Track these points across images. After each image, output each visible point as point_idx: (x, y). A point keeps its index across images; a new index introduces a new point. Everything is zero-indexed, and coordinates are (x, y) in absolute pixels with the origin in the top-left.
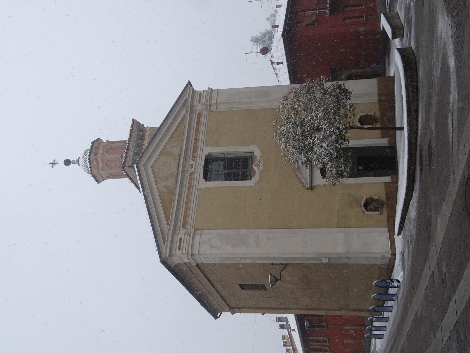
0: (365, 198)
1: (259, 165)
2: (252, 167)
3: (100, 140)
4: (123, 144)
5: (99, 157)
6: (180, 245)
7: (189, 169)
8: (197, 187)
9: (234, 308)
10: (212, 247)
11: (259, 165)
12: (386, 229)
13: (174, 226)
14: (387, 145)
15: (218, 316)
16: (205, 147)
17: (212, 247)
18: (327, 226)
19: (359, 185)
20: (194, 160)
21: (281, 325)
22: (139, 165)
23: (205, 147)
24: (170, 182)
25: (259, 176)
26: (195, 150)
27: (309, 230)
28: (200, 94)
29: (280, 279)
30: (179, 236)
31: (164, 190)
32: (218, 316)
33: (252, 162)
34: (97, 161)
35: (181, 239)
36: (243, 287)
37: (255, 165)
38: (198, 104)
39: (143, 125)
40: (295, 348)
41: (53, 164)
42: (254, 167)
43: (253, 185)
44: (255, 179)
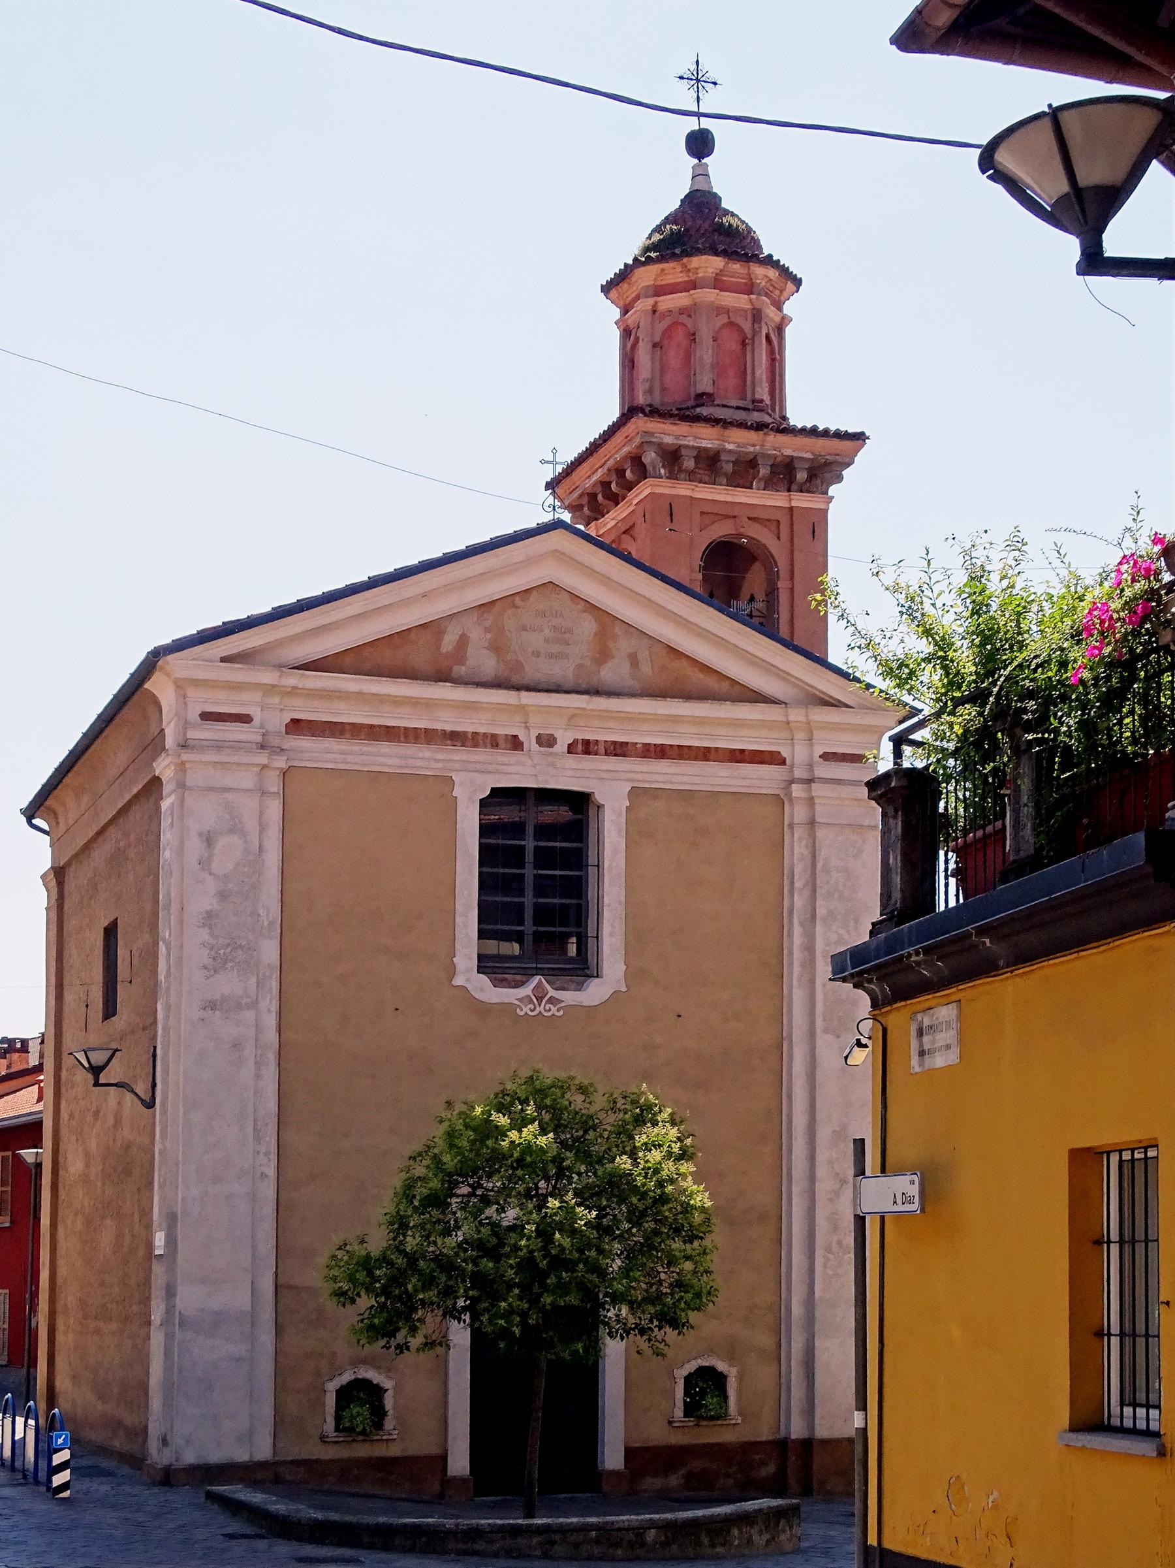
0: (388, 1384)
1: (540, 999)
2: (538, 971)
3: (790, 286)
4: (763, 393)
7: (534, 733)
8: (457, 766)
9: (60, 884)
10: (217, 833)
11: (540, 999)
12: (263, 1450)
13: (294, 688)
15: (36, 821)
16: (627, 787)
17: (209, 839)
20: (571, 749)
24: (483, 661)
25: (495, 1000)
26: (618, 750)
27: (268, 1190)
29: (97, 1084)
31: (449, 642)
33: (551, 974)
34: (692, 285)
35: (245, 719)
36: (111, 932)
38: (819, 750)
39: (839, 479)
41: (697, 79)
43: (458, 981)
44: (484, 989)
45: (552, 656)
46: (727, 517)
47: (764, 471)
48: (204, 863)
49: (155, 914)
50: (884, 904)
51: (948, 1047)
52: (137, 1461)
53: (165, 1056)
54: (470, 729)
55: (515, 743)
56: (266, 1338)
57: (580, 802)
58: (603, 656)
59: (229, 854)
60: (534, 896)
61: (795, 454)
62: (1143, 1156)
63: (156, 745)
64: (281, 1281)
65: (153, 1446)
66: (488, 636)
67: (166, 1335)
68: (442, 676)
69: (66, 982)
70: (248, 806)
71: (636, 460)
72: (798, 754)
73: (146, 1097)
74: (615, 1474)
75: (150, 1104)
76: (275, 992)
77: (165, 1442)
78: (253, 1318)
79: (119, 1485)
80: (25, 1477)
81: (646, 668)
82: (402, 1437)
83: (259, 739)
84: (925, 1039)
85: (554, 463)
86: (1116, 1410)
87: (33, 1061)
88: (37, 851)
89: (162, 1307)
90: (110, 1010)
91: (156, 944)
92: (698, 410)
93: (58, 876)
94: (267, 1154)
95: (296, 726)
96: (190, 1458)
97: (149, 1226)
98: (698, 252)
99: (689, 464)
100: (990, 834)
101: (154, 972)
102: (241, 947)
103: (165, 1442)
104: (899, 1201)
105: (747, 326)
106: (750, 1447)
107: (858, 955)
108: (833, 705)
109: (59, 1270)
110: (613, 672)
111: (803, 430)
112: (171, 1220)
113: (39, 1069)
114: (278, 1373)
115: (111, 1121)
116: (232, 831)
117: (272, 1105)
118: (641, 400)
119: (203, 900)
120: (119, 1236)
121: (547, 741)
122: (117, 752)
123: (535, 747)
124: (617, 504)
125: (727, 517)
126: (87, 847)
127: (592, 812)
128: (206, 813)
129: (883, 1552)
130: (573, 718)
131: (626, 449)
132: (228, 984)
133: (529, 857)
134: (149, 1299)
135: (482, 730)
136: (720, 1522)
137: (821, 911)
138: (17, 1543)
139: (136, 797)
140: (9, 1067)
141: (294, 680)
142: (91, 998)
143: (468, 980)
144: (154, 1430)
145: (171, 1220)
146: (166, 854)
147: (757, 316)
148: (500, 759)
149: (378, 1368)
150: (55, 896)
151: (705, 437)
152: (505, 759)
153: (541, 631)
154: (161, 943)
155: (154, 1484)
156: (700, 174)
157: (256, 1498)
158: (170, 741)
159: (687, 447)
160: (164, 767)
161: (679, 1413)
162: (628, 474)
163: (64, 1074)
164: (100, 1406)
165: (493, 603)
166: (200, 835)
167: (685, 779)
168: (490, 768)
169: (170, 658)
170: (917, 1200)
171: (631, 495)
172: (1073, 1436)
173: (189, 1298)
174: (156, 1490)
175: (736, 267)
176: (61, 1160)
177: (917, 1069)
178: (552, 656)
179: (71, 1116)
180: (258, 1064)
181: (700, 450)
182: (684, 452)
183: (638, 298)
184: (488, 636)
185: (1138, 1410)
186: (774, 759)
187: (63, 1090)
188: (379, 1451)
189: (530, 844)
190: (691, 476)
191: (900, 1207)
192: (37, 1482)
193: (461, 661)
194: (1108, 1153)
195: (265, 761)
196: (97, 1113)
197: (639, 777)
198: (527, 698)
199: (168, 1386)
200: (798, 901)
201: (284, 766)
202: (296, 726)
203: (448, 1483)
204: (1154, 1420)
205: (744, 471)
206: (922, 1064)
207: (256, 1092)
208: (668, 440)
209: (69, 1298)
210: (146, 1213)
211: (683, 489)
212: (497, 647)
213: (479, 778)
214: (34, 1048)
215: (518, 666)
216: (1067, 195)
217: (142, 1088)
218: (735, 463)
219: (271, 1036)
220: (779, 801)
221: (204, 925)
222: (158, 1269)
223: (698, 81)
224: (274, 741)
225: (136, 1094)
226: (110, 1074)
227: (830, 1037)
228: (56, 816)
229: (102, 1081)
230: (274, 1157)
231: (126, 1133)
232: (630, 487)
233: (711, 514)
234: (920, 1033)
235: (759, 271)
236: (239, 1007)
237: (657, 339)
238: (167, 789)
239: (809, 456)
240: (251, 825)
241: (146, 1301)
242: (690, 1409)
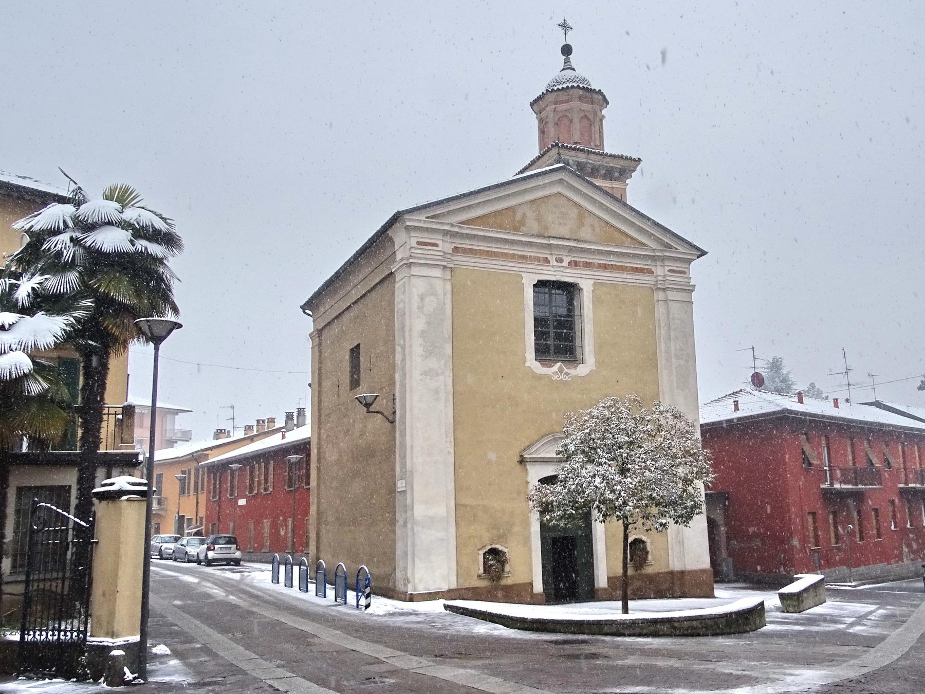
0: (506, 550)
1: (561, 373)
2: (558, 361)
11: (561, 373)
12: (454, 586)
15: (307, 311)
23: (592, 282)
26: (588, 265)
28: (684, 273)
29: (368, 412)
31: (519, 216)
35: (436, 245)
41: (565, 26)
42: (559, 364)
45: (560, 224)
48: (420, 308)
59: (431, 303)
70: (439, 284)
74: (604, 589)
88: (308, 324)
93: (319, 333)
95: (456, 249)
105: (591, 117)
116: (432, 294)
121: (560, 261)
132: (432, 363)
136: (18, 518)
137: (673, 336)
139: (377, 284)
147: (595, 114)
200: (663, 332)
203: (533, 595)
212: (539, 219)
215: (546, 228)
236: (437, 374)
240: (440, 292)
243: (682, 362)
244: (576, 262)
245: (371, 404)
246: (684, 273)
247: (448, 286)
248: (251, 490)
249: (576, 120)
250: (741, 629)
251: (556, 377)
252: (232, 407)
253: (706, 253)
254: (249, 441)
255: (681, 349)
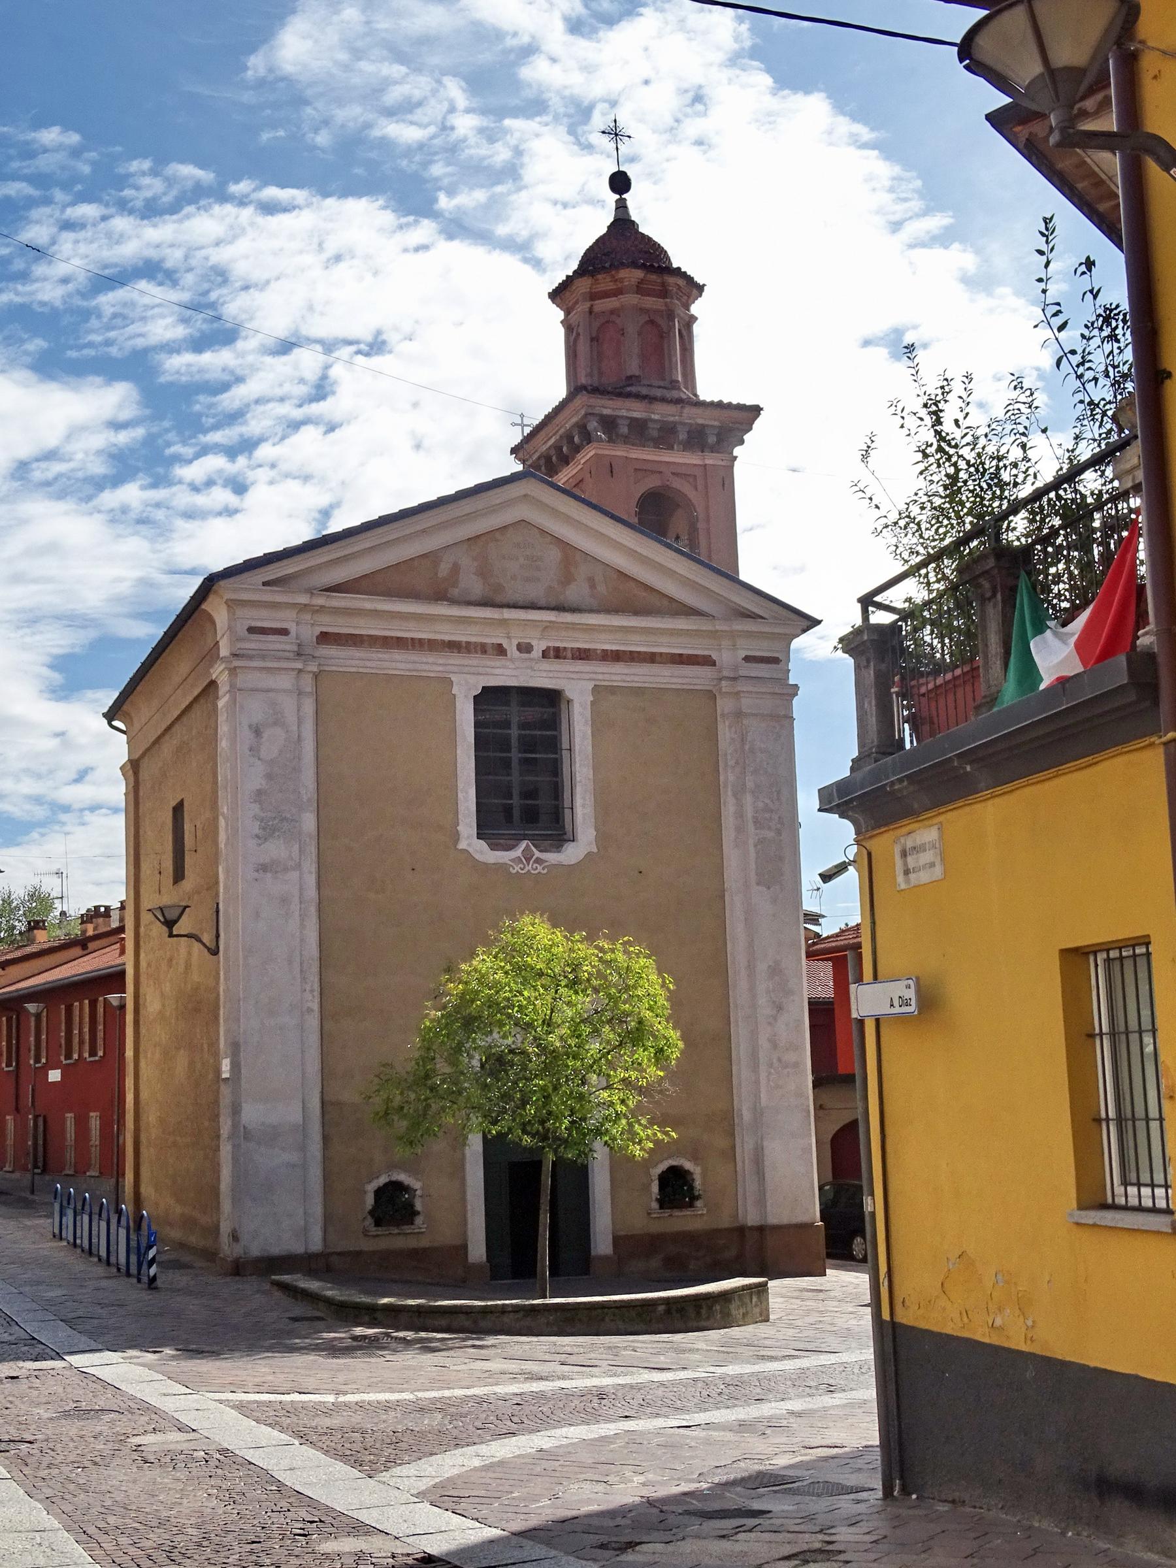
0: (416, 1185)
1: (528, 860)
2: (520, 838)
3: (695, 291)
5: (631, 299)
6: (263, 631)
7: (515, 642)
8: (455, 669)
9: (136, 773)
11: (528, 860)
12: (316, 1243)
13: (322, 607)
14: (593, 1253)
15: (116, 723)
16: (591, 685)
17: (257, 732)
18: (326, 1073)
19: (458, 1171)
20: (545, 654)
21: (1034, 625)
22: (524, 481)
25: (492, 861)
26: (582, 655)
27: (313, 1022)
28: (776, 661)
29: (171, 935)
30: (293, 628)
31: (444, 569)
32: (116, 723)
35: (284, 632)
36: (178, 810)
37: (528, 845)
38: (743, 654)
39: (741, 442)
40: (92, 946)
42: (524, 844)
43: (462, 845)
44: (481, 851)
46: (653, 472)
47: (682, 436)
49: (215, 792)
50: (861, 745)
51: (932, 865)
52: (210, 1255)
53: (226, 911)
54: (464, 639)
55: (500, 650)
56: (315, 1147)
57: (552, 698)
58: (567, 578)
60: (521, 775)
61: (706, 422)
62: (1117, 955)
63: (212, 655)
64: (326, 1098)
65: (225, 1239)
66: (476, 564)
67: (234, 1146)
68: (440, 596)
69: (142, 852)
70: (288, 705)
71: (582, 428)
72: (726, 657)
73: (212, 946)
74: (605, 1259)
75: (215, 952)
76: (314, 858)
77: (235, 1237)
78: (305, 1127)
79: (196, 1275)
80: (119, 1270)
81: (601, 589)
82: (427, 1231)
83: (295, 648)
84: (909, 859)
85: (523, 426)
86: (1120, 1190)
87: (115, 924)
89: (230, 1123)
90: (179, 875)
91: (216, 819)
92: (629, 389)
93: (133, 768)
94: (312, 991)
95: (325, 638)
96: (255, 1251)
97: (216, 1055)
98: (623, 265)
99: (624, 430)
100: (941, 686)
101: (216, 843)
102: (285, 819)
103: (235, 1237)
104: (896, 1003)
106: (716, 1232)
107: (841, 787)
108: (749, 616)
109: (141, 1095)
110: (575, 592)
111: (712, 404)
112: (235, 1049)
113: (121, 929)
114: (327, 1176)
115: (181, 968)
117: (315, 952)
118: (583, 380)
119: (255, 779)
120: (192, 1063)
121: (524, 648)
122: (180, 665)
123: (517, 654)
124: (568, 464)
125: (653, 472)
126: (157, 741)
127: (563, 706)
128: (255, 709)
129: (894, 1325)
130: (548, 627)
131: (574, 420)
132: (276, 849)
133: (514, 743)
134: (218, 1116)
135: (473, 639)
137: (750, 784)
138: (115, 1329)
140: (95, 929)
141: (320, 601)
142: (163, 865)
143: (469, 845)
144: (225, 1228)
145: (235, 1049)
146: (223, 744)
148: (489, 663)
149: (405, 1171)
150: (132, 779)
151: (635, 410)
152: (492, 664)
153: (517, 559)
154: (221, 818)
155: (226, 1275)
156: (621, 206)
157: (313, 1285)
158: (224, 652)
159: (622, 417)
160: (219, 672)
161: (655, 1205)
162: (576, 439)
163: (142, 929)
164: (179, 1210)
165: (478, 537)
166: (250, 726)
167: (636, 679)
168: (481, 670)
169: (222, 583)
170: (913, 1002)
171: (579, 456)
172: (1083, 1213)
173: (252, 1114)
174: (228, 1279)
175: (653, 277)
176: (141, 1002)
177: (903, 886)
178: (528, 580)
179: (149, 965)
180: (303, 917)
181: (633, 420)
182: (620, 421)
183: (576, 303)
184: (476, 564)
185: (1129, 1188)
186: (707, 661)
187: (142, 943)
188: (412, 1243)
189: (514, 732)
190: (626, 440)
191: (897, 1010)
192: (128, 1274)
193: (455, 584)
194: (1095, 953)
195: (299, 665)
196: (170, 960)
197: (600, 677)
198: (508, 614)
199: (235, 1188)
201: (315, 669)
202: (325, 638)
203: (470, 1268)
204: (1161, 1198)
205: (666, 436)
206: (907, 881)
207: (302, 940)
208: (606, 412)
209: (151, 1117)
210: (213, 1044)
211: (620, 451)
212: (484, 573)
213: (472, 679)
214: (115, 915)
215: (499, 588)
216: (1042, 75)
217: (207, 938)
218: (660, 430)
219: (312, 893)
220: (711, 696)
221: (255, 801)
222: (225, 1090)
223: (616, 135)
224: (308, 651)
225: (204, 945)
226: (181, 927)
227: (760, 888)
228: (131, 719)
229: (175, 933)
230: (317, 994)
231: (195, 977)
232: (577, 449)
233: (643, 470)
234: (904, 854)
235: (671, 280)
236: (286, 870)
237: (594, 335)
238: (221, 691)
239: (716, 423)
240: (291, 719)
241: (216, 1117)
242: (663, 1203)
243: (770, 834)
244: (557, 649)
245: (175, 922)
246: (776, 661)
247: (309, 707)
248: (68, 1056)
249: (632, 329)
250: (703, 1323)
251: (517, 868)
252: (59, 874)
253: (819, 622)
254: (77, 951)
255: (767, 809)
